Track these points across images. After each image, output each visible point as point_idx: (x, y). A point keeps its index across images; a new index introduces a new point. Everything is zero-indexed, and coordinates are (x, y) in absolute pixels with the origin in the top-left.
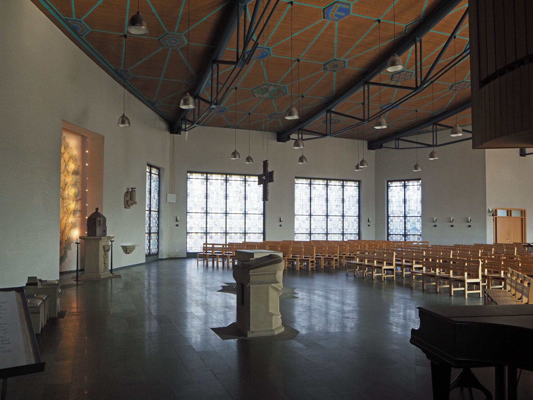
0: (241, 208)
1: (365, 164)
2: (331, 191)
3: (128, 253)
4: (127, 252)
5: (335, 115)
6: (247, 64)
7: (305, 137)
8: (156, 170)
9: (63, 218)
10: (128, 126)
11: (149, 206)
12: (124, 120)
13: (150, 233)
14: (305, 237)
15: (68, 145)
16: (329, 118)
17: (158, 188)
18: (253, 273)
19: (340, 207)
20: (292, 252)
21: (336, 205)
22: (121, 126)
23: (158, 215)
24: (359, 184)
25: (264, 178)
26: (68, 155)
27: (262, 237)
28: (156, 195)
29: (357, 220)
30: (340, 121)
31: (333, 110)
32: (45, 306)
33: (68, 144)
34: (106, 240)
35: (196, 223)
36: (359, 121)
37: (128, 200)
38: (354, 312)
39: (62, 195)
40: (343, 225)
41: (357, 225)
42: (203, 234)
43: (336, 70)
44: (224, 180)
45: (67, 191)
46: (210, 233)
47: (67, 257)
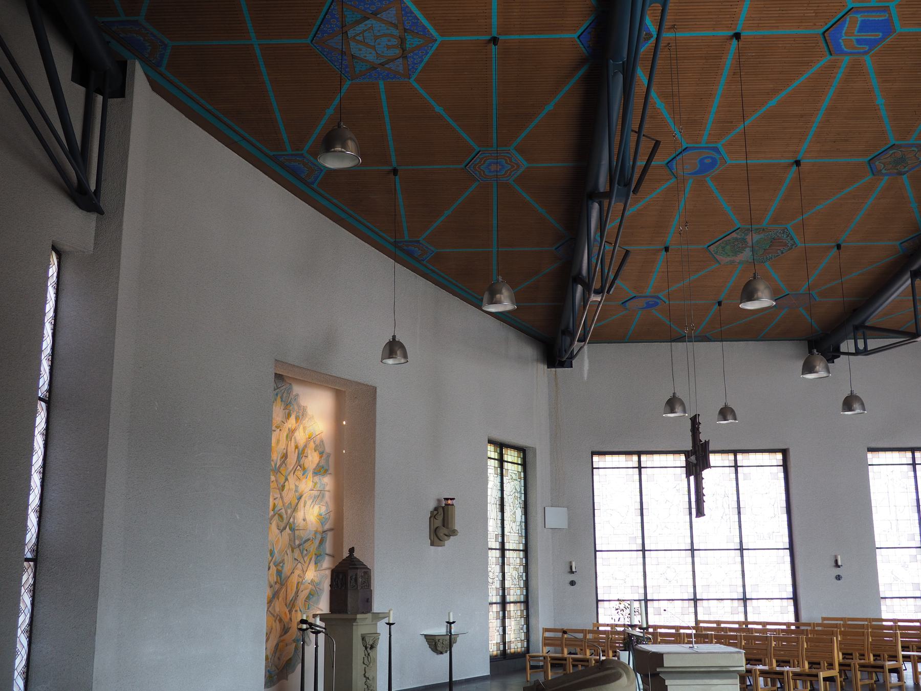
3: (441, 653)
4: (438, 648)
6: (635, 191)
7: (873, 344)
9: (293, 572)
11: (500, 539)
13: (503, 603)
14: (912, 608)
17: (523, 495)
22: (390, 361)
26: (304, 432)
28: (519, 512)
33: (305, 409)
34: (369, 621)
37: (437, 527)
39: (291, 520)
43: (906, 169)
45: (302, 511)
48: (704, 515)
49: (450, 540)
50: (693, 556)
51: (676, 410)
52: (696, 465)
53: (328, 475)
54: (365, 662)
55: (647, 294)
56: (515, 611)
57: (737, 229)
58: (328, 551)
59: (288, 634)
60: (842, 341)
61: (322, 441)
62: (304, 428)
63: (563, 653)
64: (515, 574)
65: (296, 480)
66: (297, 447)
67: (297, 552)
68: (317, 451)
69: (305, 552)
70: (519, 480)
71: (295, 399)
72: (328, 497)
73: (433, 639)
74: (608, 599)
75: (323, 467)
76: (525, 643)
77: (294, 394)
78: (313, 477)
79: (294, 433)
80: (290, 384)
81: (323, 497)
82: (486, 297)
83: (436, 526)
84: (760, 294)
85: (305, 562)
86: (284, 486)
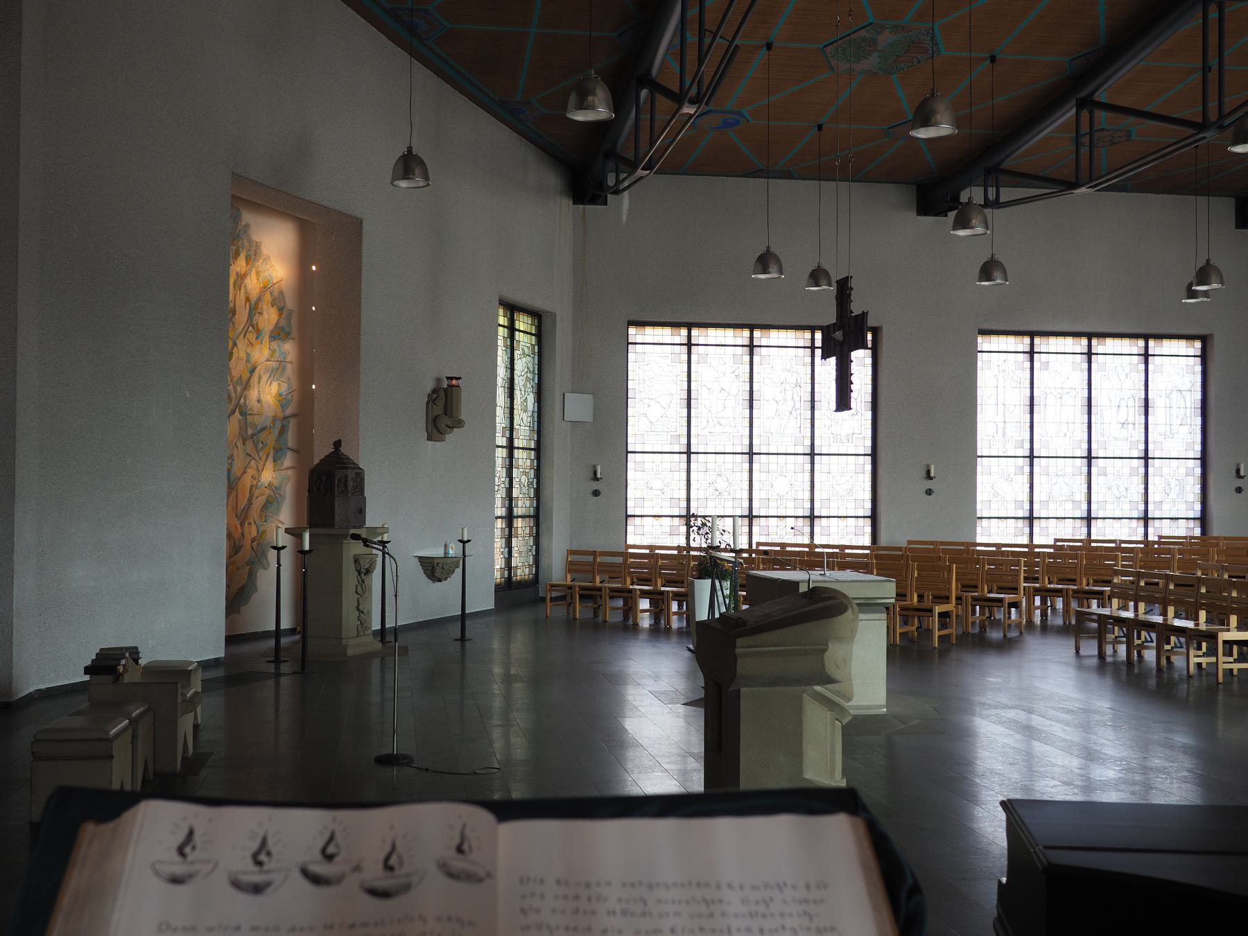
0: (800, 435)
1: (1214, 278)
2: (1103, 373)
3: (440, 580)
5: (1111, 115)
7: (1007, 194)
8: (530, 319)
9: (245, 472)
10: (421, 184)
12: (409, 164)
13: (510, 518)
15: (258, 251)
16: (1085, 129)
18: (747, 647)
19: (1134, 429)
20: (988, 577)
21: (1122, 420)
22: (403, 184)
23: (535, 461)
24: (1204, 349)
25: (839, 335)
26: (258, 279)
27: (868, 530)
28: (531, 399)
29: (1198, 471)
30: (1129, 136)
31: (1101, 96)
32: (134, 737)
33: (258, 246)
35: (657, 484)
36: (1190, 131)
37: (437, 416)
38: (1123, 787)
40: (1146, 489)
41: (1197, 489)
42: (1192, 521)
44: (1138, 355)
45: (256, 390)
46: (984, 518)
47: (257, 591)
48: (851, 409)
49: (453, 433)
50: (751, 462)
51: (770, 270)
52: (842, 344)
53: (290, 341)
54: (358, 592)
55: (728, 108)
56: (523, 528)
57: (868, 25)
58: (290, 444)
59: (240, 554)
60: (965, 187)
61: (281, 293)
62: (258, 273)
63: (594, 581)
64: (524, 479)
65: (248, 346)
66: (248, 299)
67: (250, 445)
68: (275, 307)
69: (260, 445)
70: (532, 356)
71: (245, 231)
72: (290, 370)
73: (430, 563)
74: (640, 514)
75: (283, 329)
76: (534, 569)
77: (243, 223)
78: (270, 342)
79: (244, 280)
80: (238, 209)
81: (284, 369)
82: (573, 99)
83: (435, 415)
84: (939, 117)
85: (260, 459)
86: (232, 353)
